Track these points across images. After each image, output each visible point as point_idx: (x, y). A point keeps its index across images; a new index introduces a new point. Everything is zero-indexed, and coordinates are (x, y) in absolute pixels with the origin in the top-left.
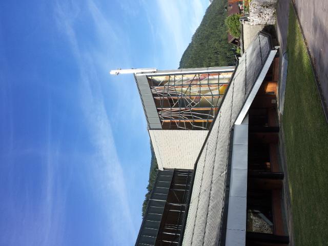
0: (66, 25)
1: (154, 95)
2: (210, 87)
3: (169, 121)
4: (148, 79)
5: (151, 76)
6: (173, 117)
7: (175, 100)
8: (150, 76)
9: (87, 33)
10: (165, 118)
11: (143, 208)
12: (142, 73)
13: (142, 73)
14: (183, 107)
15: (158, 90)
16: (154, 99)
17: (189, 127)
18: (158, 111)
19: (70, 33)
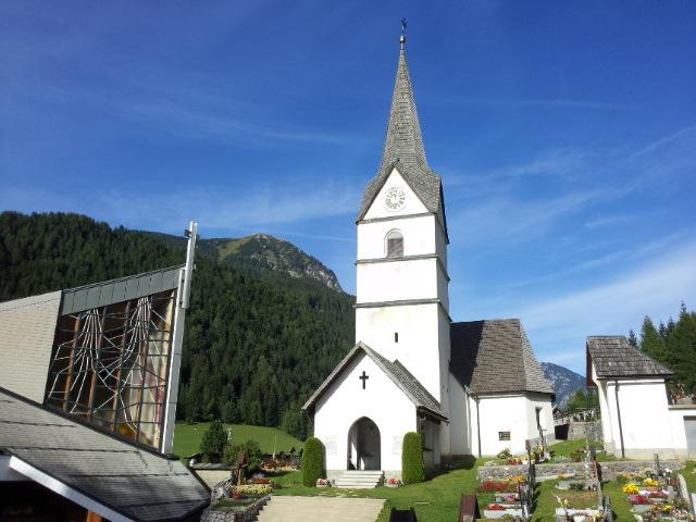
0: (551, 163)
1: (134, 302)
2: (135, 407)
3: (76, 329)
4: (171, 291)
5: (175, 298)
6: (83, 337)
7: (118, 342)
8: (176, 294)
9: (540, 188)
10: (82, 322)
11: (77, 216)
12: (183, 281)
13: (183, 281)
14: (101, 357)
15: (144, 310)
16: (126, 302)
17: (55, 366)
18: (101, 309)
19: (536, 167)
